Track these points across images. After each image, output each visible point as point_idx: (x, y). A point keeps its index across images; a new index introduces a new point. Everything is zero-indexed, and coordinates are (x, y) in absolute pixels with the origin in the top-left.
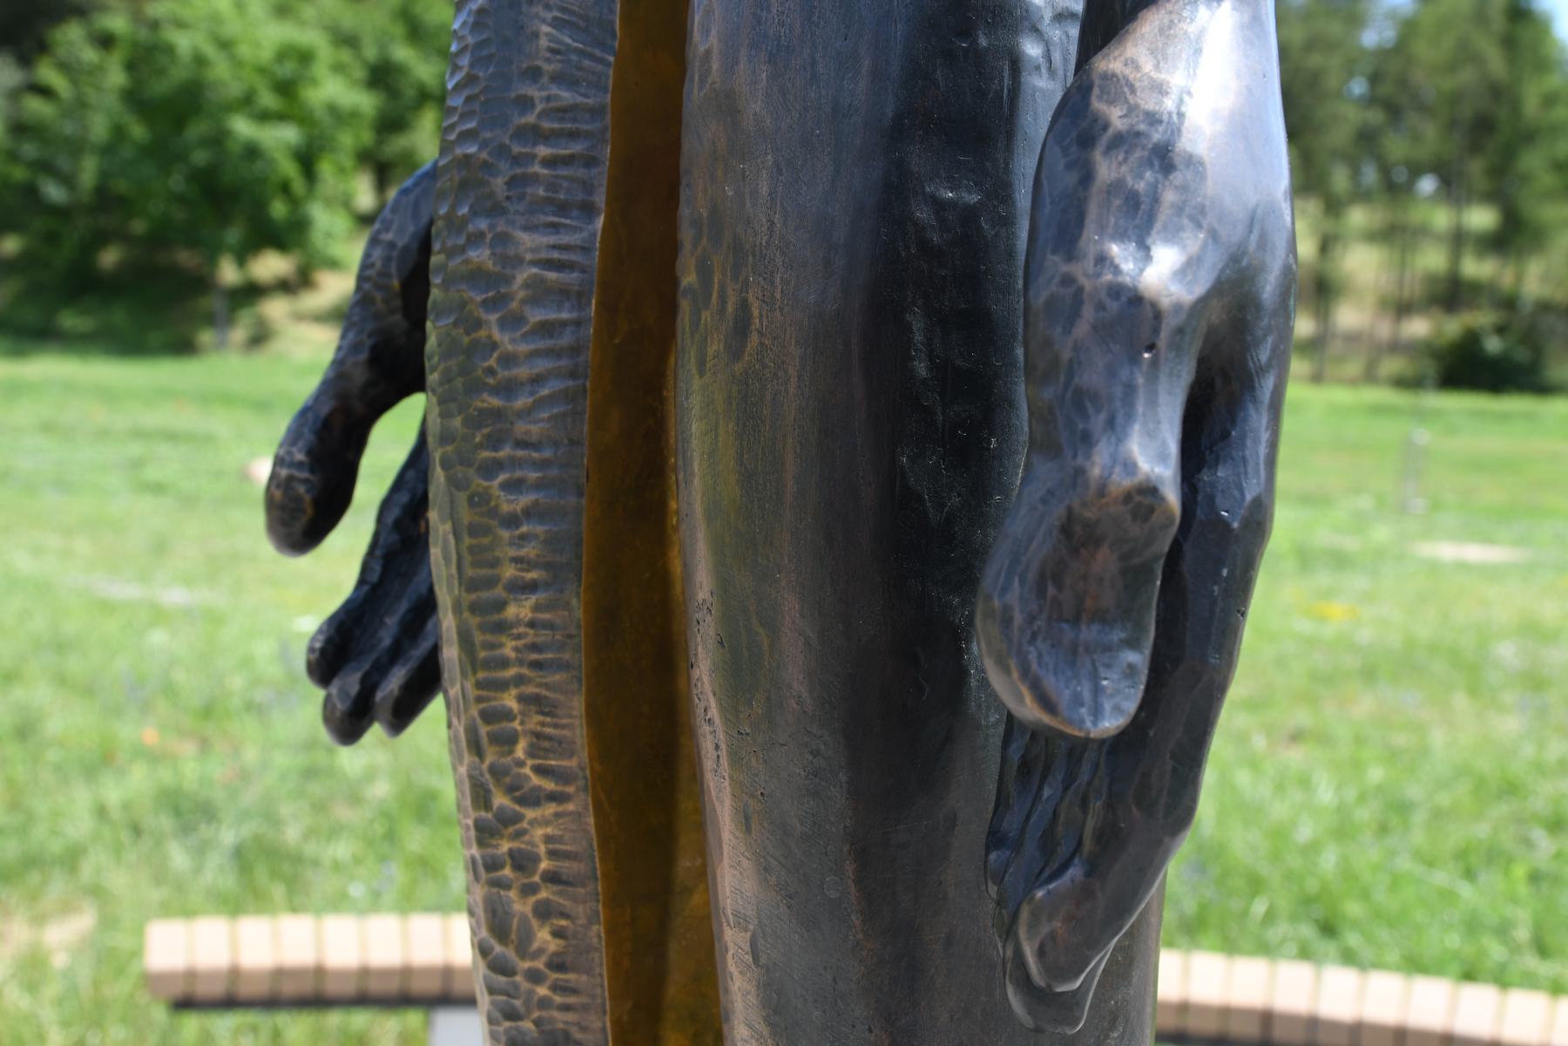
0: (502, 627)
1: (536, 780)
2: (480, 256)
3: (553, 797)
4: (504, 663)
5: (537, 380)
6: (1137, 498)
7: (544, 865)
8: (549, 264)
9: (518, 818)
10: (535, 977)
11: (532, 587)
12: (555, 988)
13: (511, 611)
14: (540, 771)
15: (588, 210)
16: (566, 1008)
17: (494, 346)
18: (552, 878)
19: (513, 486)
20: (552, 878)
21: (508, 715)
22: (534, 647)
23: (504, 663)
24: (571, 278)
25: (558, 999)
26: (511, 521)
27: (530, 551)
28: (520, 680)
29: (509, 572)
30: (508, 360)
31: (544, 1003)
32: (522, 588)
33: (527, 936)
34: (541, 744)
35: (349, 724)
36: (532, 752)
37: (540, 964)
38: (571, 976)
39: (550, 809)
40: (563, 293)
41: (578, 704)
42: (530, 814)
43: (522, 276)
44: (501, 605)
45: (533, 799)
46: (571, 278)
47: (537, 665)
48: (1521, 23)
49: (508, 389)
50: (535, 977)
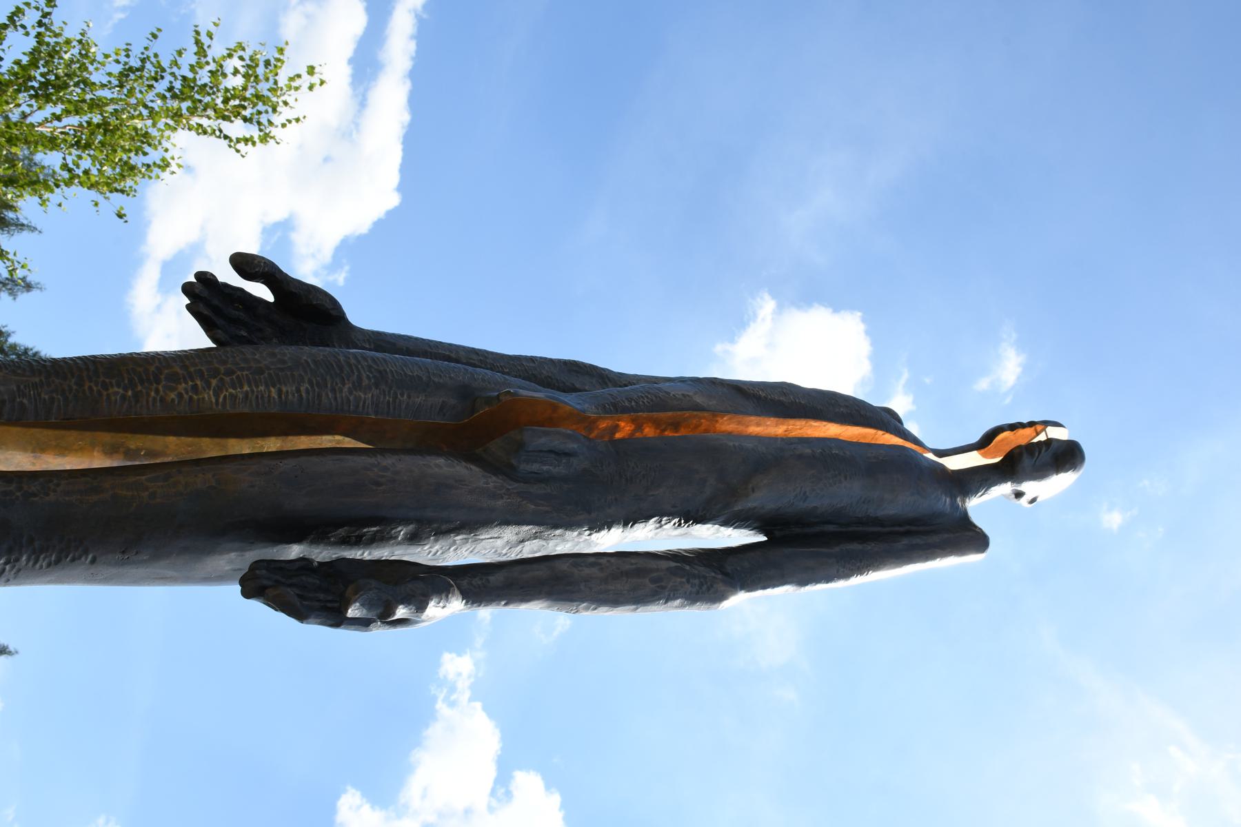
0: (267, 386)
2: (365, 382)
3: (217, 401)
5: (336, 399)
6: (54, 443)
9: (209, 388)
10: (157, 391)
11: (280, 397)
14: (225, 397)
15: (376, 413)
17: (344, 384)
18: (191, 398)
19: (307, 391)
20: (191, 398)
21: (241, 387)
23: (257, 386)
24: (361, 409)
26: (298, 390)
29: (284, 389)
30: (341, 391)
31: (148, 395)
32: (280, 392)
33: (173, 389)
34: (234, 397)
35: (187, 289)
36: (231, 394)
40: (357, 407)
41: (246, 410)
45: (217, 395)
46: (361, 409)
49: (333, 390)
50: (157, 391)
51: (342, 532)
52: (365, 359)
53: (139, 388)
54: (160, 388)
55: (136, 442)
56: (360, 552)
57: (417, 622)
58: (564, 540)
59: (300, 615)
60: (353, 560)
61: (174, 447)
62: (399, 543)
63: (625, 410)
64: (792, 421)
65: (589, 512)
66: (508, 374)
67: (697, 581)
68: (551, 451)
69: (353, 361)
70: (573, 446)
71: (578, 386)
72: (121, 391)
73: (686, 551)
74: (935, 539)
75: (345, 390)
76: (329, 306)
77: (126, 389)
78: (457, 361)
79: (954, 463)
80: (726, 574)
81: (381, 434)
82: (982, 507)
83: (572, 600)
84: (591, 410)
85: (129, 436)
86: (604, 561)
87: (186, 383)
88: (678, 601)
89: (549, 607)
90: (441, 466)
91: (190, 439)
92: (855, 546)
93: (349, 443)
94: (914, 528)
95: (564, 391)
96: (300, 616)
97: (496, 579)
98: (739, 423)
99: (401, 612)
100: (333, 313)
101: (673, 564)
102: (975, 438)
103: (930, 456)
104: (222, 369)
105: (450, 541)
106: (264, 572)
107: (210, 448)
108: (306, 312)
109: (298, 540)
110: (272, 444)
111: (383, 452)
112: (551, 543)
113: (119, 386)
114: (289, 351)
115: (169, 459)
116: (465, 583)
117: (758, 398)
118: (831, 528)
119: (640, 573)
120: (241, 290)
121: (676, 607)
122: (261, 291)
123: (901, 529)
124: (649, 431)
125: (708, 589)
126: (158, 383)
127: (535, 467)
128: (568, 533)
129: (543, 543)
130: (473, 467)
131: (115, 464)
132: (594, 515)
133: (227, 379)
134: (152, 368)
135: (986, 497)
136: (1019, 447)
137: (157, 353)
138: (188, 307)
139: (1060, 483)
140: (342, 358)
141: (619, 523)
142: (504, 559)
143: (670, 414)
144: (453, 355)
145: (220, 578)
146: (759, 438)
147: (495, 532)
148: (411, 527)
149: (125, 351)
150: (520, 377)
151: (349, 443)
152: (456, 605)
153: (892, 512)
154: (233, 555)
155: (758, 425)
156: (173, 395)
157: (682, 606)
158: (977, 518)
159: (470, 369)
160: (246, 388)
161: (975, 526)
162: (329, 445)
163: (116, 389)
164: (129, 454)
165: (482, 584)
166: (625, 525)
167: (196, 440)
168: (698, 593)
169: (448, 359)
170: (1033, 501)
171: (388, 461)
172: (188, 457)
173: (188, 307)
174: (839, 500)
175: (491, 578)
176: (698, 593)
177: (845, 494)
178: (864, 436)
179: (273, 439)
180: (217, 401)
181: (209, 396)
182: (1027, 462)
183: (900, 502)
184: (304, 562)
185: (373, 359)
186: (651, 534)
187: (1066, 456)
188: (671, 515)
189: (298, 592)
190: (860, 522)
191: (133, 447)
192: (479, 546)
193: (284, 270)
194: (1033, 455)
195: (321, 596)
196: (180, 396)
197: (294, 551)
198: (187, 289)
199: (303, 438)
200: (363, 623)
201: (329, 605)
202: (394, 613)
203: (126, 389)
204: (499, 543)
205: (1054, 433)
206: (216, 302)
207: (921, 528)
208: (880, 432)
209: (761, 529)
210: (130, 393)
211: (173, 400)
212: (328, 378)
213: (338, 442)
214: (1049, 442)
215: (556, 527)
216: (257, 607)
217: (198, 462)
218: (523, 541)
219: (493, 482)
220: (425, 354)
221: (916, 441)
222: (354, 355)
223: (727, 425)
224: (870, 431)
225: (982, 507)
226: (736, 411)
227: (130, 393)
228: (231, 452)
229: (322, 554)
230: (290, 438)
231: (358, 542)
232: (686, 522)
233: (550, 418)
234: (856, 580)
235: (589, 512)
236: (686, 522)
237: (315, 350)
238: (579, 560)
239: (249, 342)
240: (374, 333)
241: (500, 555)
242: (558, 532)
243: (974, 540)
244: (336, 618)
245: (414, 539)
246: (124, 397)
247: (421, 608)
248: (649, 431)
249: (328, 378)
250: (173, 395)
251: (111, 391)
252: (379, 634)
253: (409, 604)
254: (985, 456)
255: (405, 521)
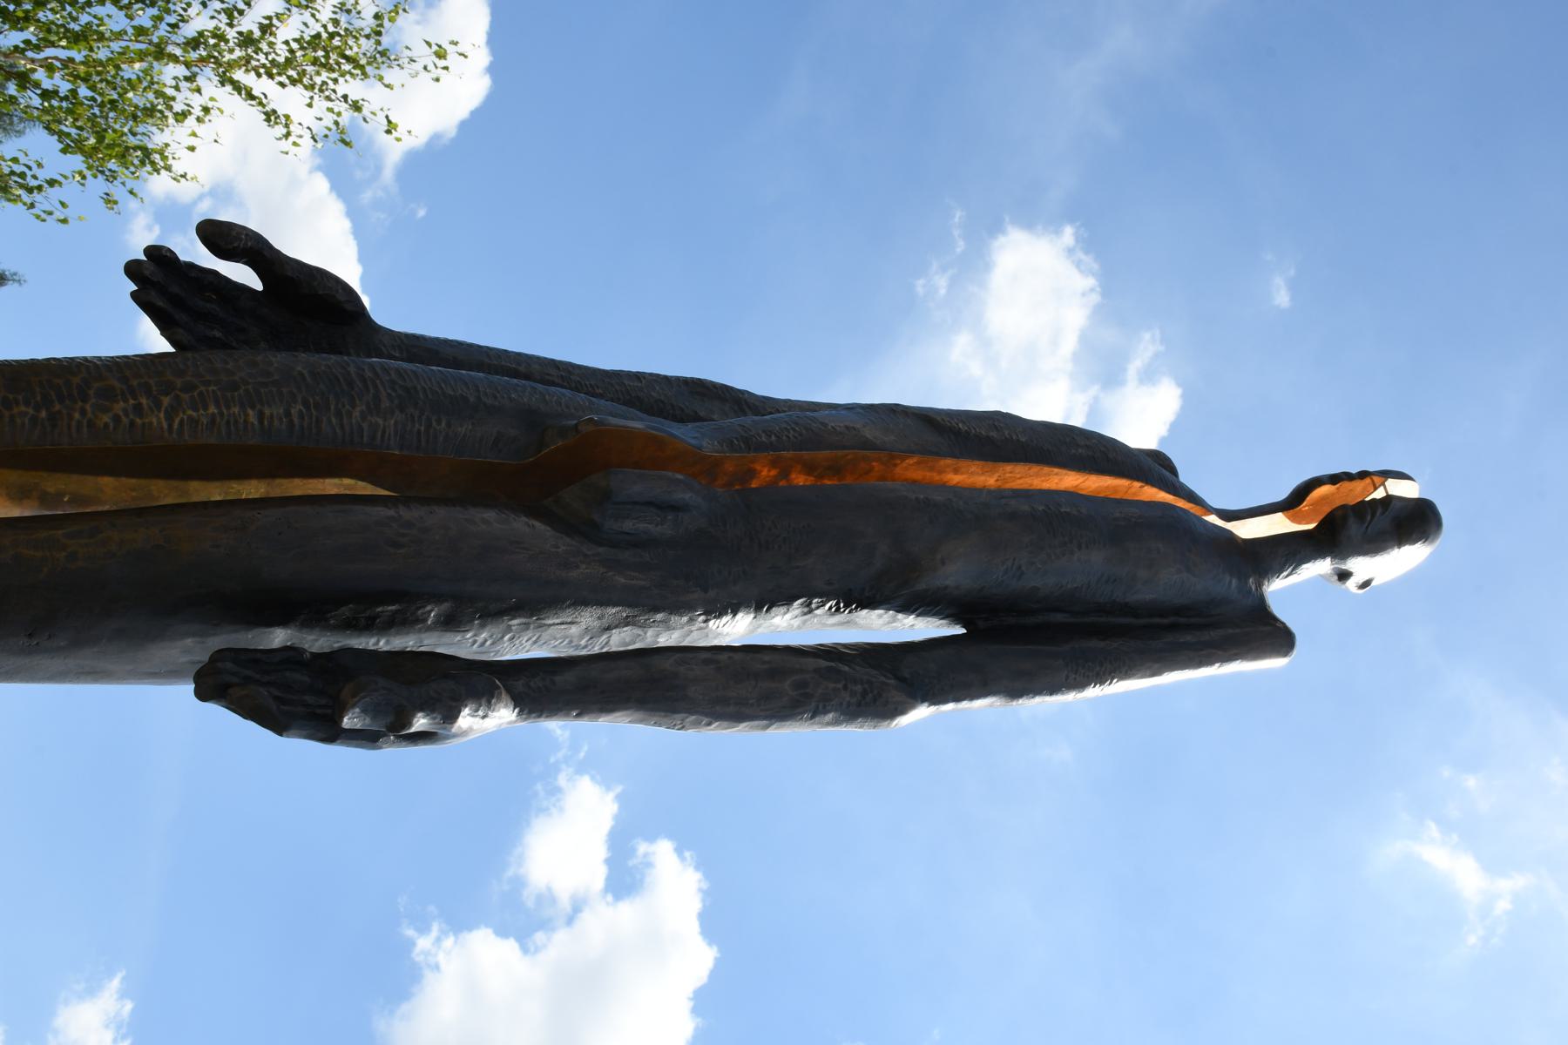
1: (177, 421)
2: (385, 404)
3: (170, 426)
4: (228, 408)
5: (342, 427)
7: (139, 421)
8: (384, 432)
10: (83, 412)
12: (79, 422)
13: (250, 412)
14: (182, 421)
16: (69, 427)
17: (354, 407)
18: (132, 423)
20: (132, 423)
21: (206, 408)
22: (236, 422)
23: (228, 408)
25: (74, 423)
26: (288, 414)
27: (276, 423)
28: (221, 414)
29: (267, 412)
30: (350, 414)
31: (70, 417)
32: (261, 415)
34: (194, 422)
35: (132, 269)
36: (190, 417)
37: (90, 415)
38: (85, 429)
39: (165, 426)
41: (212, 441)
42: (162, 415)
43: (380, 422)
44: (253, 407)
45: (170, 419)
47: (228, 422)
48: (115, 1041)
49: (339, 414)
50: (83, 412)
51: (346, 611)
52: (386, 370)
53: (57, 407)
54: (88, 407)
55: (54, 483)
56: (373, 641)
57: (447, 737)
58: (669, 628)
59: (278, 724)
60: (364, 651)
61: (111, 491)
62: (429, 629)
63: (762, 447)
64: (1009, 467)
65: (706, 590)
66: (601, 396)
67: (859, 688)
68: (650, 504)
69: (368, 374)
70: (686, 496)
71: (702, 414)
72: (31, 411)
73: (845, 646)
74: (1214, 634)
75: (356, 413)
76: (341, 297)
77: (37, 408)
78: (527, 377)
79: (1248, 530)
80: (902, 680)
81: (408, 477)
82: (1284, 591)
83: (674, 711)
84: (709, 446)
85: (45, 474)
86: (723, 657)
87: (126, 401)
88: (831, 716)
89: (640, 721)
90: (488, 521)
91: (134, 481)
92: (1095, 644)
93: (364, 488)
94: (1182, 620)
95: (681, 421)
96: (279, 727)
97: (566, 679)
98: (932, 469)
99: (420, 723)
100: (349, 307)
101: (823, 663)
102: (1282, 494)
103: (1213, 519)
104: (179, 382)
105: (502, 626)
106: (229, 665)
107: (165, 492)
108: (307, 305)
109: (283, 622)
110: (253, 489)
111: (406, 501)
112: (650, 632)
113: (27, 404)
114: (279, 359)
115: (106, 508)
116: (520, 685)
117: (957, 433)
118: (1059, 618)
119: (775, 673)
120: (215, 273)
121: (828, 724)
122: (243, 274)
123: (1165, 621)
124: (800, 479)
125: (875, 700)
126: (85, 401)
127: (628, 525)
128: (674, 619)
129: (639, 631)
130: (537, 524)
131: (27, 513)
132: (712, 594)
133: (185, 397)
134: (76, 380)
135: (1294, 579)
136: (1343, 507)
137: (85, 359)
138: (134, 295)
139: (1405, 559)
140: (352, 369)
141: (748, 606)
142: (584, 652)
143: (826, 453)
144: (522, 369)
145: (169, 674)
146: (957, 490)
147: (566, 616)
148: (446, 606)
149: (130, 352)
150: (618, 401)
151: (364, 488)
152: (504, 715)
153: (1149, 597)
154: (189, 641)
155: (956, 471)
156: (106, 418)
157: (836, 723)
158: (1278, 609)
159: (540, 387)
160: (212, 409)
161: (1275, 619)
162: (334, 491)
163: (23, 408)
164: (44, 499)
165: (544, 689)
166: (758, 609)
167: (143, 482)
168: (859, 705)
169: (515, 374)
170: (1366, 584)
171: (406, 514)
172: (122, 506)
173: (134, 295)
174: (1070, 574)
175: (557, 678)
176: (859, 705)
177: (1081, 570)
178: (1115, 489)
179: (254, 482)
180: (170, 426)
181: (158, 419)
182: (1354, 528)
183: (1168, 580)
184: (291, 656)
185: (397, 371)
186: (796, 622)
187: (1416, 521)
188: (826, 596)
189: (276, 693)
190: (1179, 611)
191: (51, 490)
192: (546, 635)
193: (277, 246)
194: (1357, 520)
195: (309, 699)
196: (117, 419)
197: (279, 637)
198: (132, 269)
199: (297, 481)
200: (367, 738)
201: (319, 711)
202: (410, 724)
203: (37, 408)
204: (574, 630)
205: (1397, 488)
206: (175, 289)
207: (1193, 620)
208: (1137, 484)
209: (956, 618)
210: (44, 414)
211: (106, 425)
212: (331, 398)
213: (348, 487)
214: (1389, 499)
215: (656, 610)
216: (218, 715)
217: (140, 512)
218: (609, 628)
219: (565, 544)
220: (457, 364)
221: (1192, 497)
222: (371, 366)
223: (911, 469)
224: (1122, 483)
225: (1284, 591)
226: (930, 452)
227: (44, 414)
228: (195, 499)
229: (318, 642)
230: (278, 481)
231: (370, 626)
232: (846, 606)
233: (654, 455)
234: (1093, 692)
235: (706, 590)
236: (846, 606)
237: (315, 358)
238: (690, 655)
239: (225, 346)
240: (407, 336)
241: (577, 647)
242: (659, 616)
243: (1277, 638)
244: (329, 731)
245: (450, 623)
246: (34, 420)
247: (451, 716)
248: (800, 479)
249: (331, 398)
250: (106, 418)
251: (15, 410)
252: (392, 757)
253: (433, 711)
254: (1294, 519)
255: (437, 598)
